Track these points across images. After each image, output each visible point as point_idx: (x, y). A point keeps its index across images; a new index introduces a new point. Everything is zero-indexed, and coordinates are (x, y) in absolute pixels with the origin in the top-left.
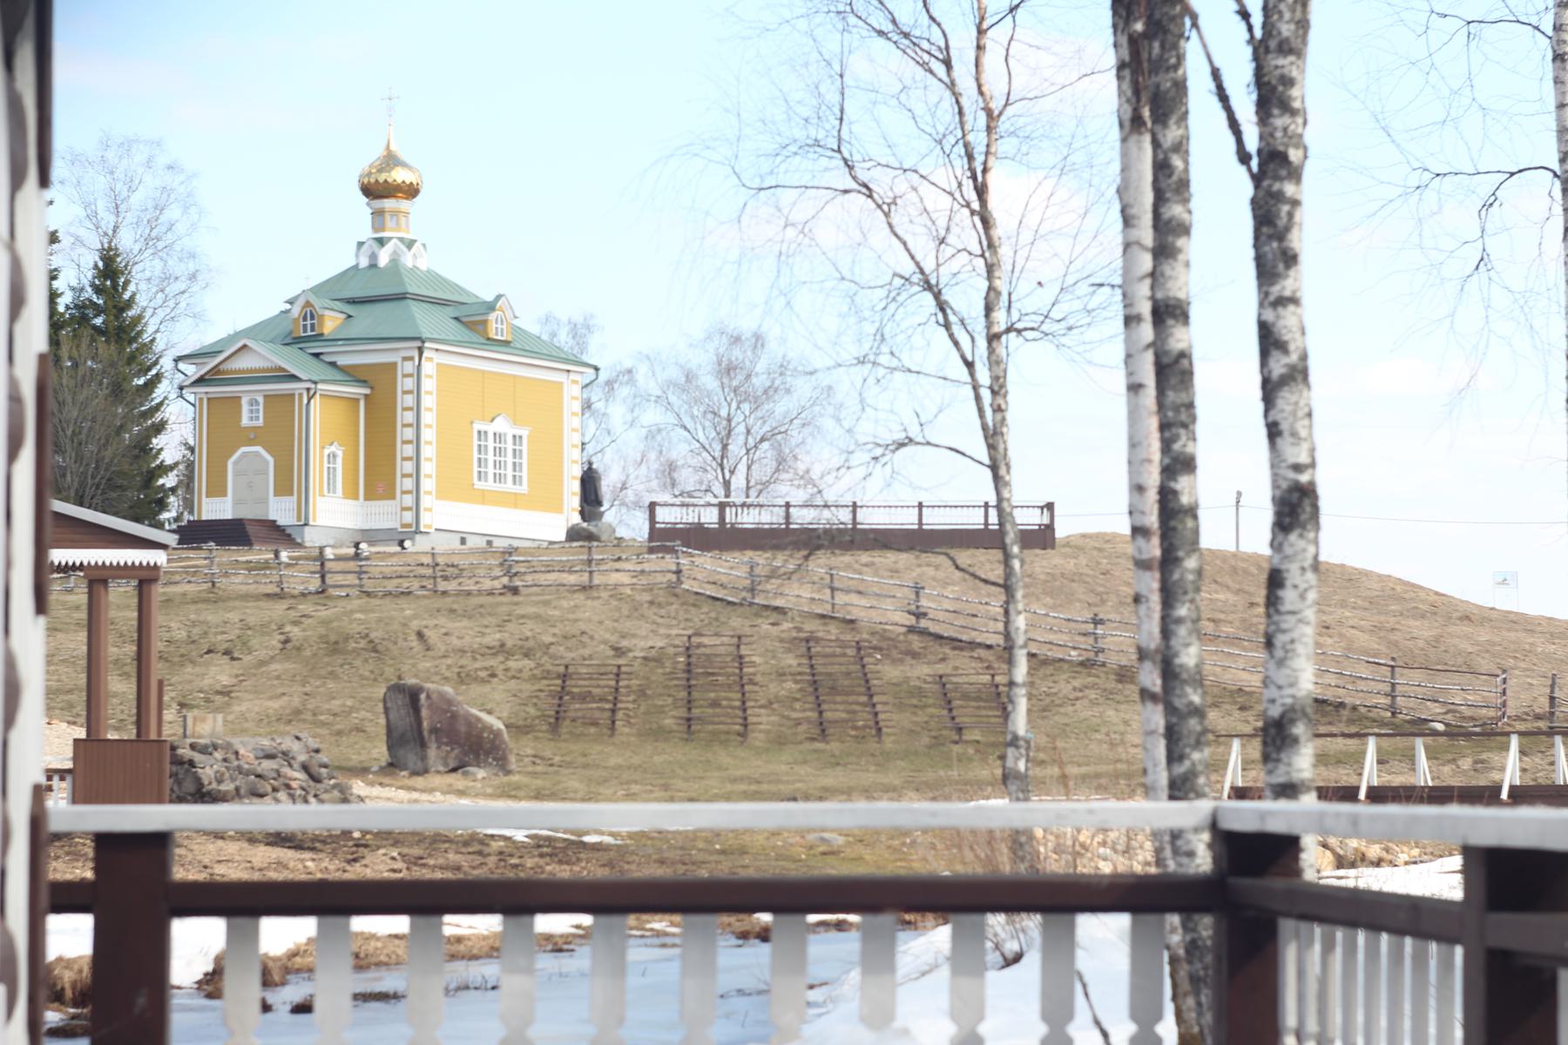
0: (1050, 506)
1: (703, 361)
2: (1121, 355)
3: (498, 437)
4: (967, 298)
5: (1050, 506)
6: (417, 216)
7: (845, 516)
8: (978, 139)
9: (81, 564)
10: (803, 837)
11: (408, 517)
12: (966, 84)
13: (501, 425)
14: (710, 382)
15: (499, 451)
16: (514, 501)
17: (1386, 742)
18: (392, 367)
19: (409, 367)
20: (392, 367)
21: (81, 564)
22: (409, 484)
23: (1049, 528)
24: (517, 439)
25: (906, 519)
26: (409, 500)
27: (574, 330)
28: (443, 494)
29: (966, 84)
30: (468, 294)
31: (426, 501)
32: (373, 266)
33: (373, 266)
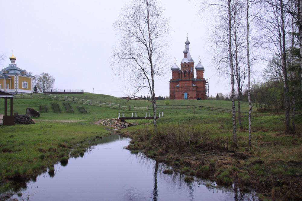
0: (83, 90)
1: (42, 76)
2: (250, 76)
3: (25, 83)
4: (148, 70)
5: (83, 90)
6: (16, 62)
7: (57, 91)
8: (150, 53)
9: (145, 97)
10: (222, 126)
11: (16, 91)
12: (148, 46)
13: (25, 82)
14: (43, 78)
15: (25, 85)
16: (26, 89)
17: (138, 113)
18: (14, 76)
19: (16, 76)
20: (14, 76)
21: (145, 97)
22: (16, 88)
23: (83, 92)
24: (26, 83)
25: (63, 91)
26: (16, 89)
27: (30, 73)
28: (19, 89)
29: (148, 46)
30: (20, 69)
31: (18, 89)
32: (11, 66)
33: (11, 66)
